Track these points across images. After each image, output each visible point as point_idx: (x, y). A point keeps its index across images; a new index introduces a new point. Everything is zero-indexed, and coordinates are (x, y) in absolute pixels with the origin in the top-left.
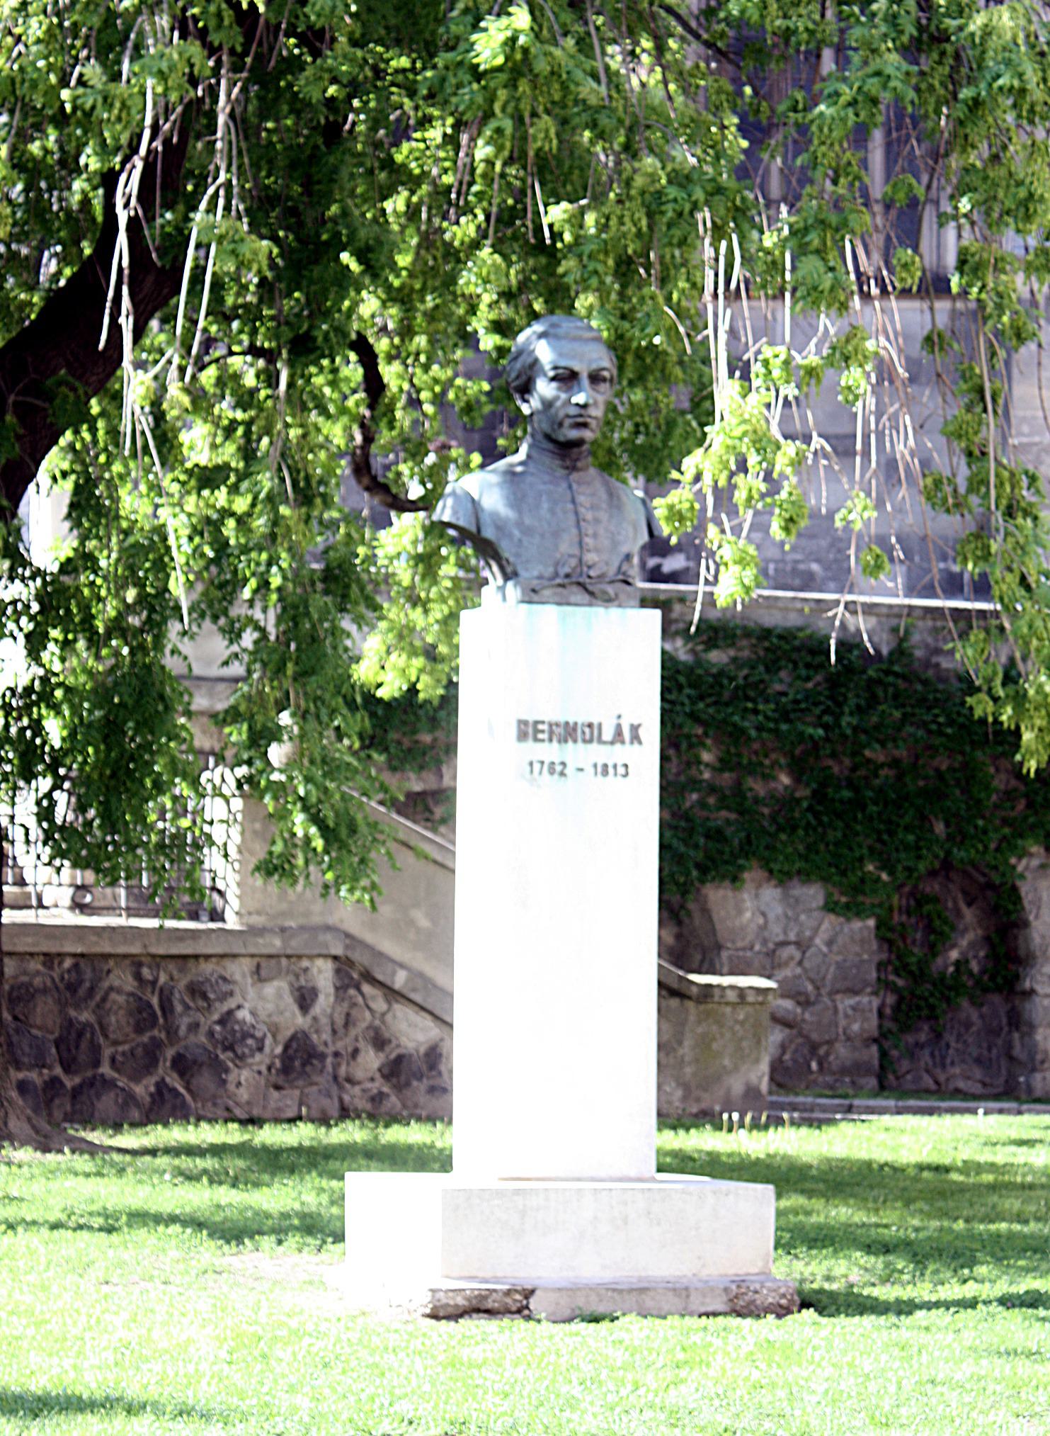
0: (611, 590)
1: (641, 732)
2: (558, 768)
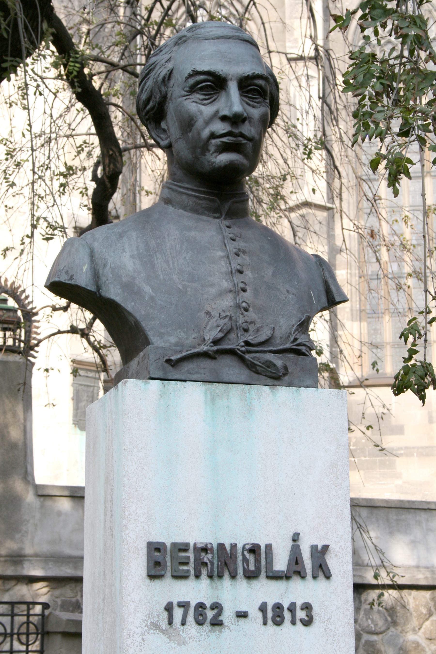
0: (278, 361)
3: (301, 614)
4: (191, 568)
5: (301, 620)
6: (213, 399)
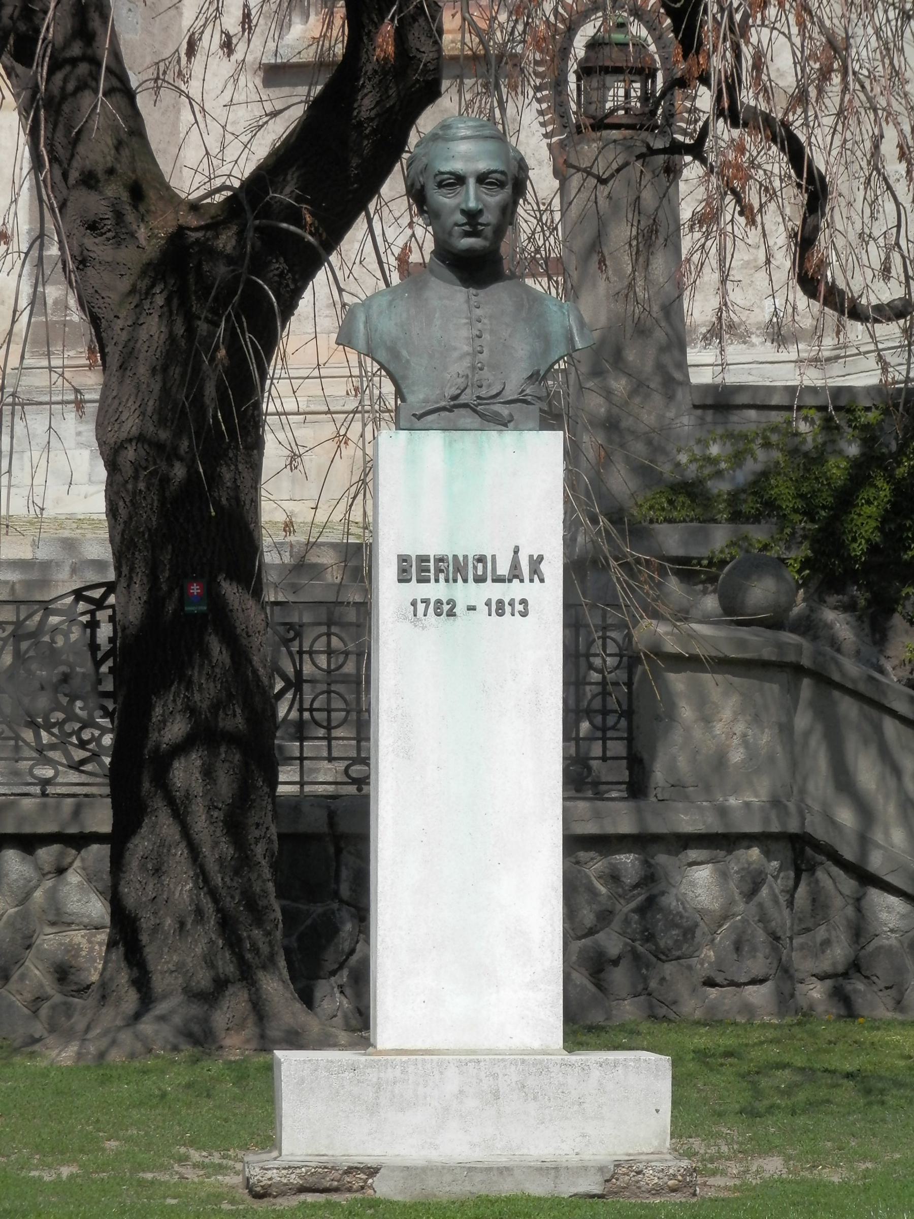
0: (505, 411)
1: (543, 567)
2: (446, 608)
3: (521, 608)
5: (519, 612)
6: (450, 443)
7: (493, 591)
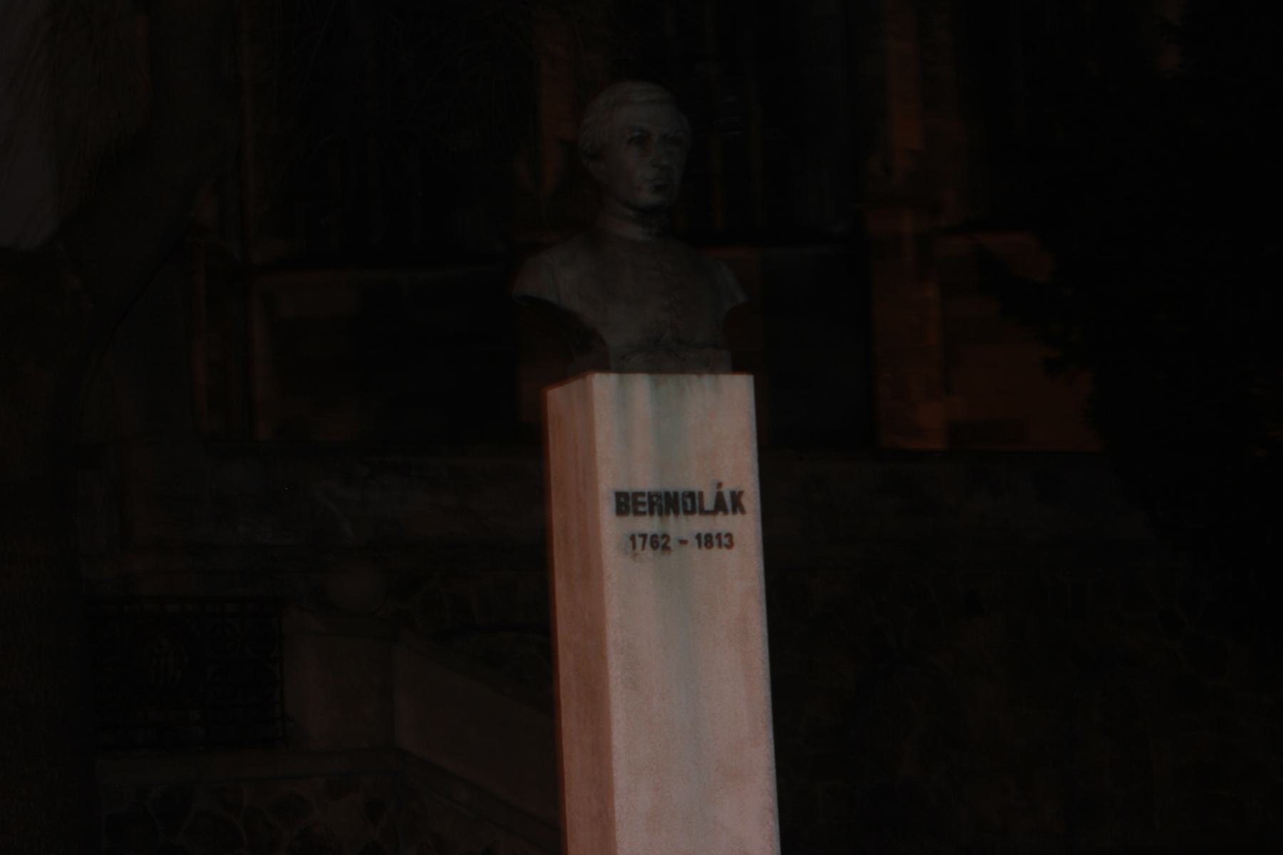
4: (646, 508)
7: (699, 524)
